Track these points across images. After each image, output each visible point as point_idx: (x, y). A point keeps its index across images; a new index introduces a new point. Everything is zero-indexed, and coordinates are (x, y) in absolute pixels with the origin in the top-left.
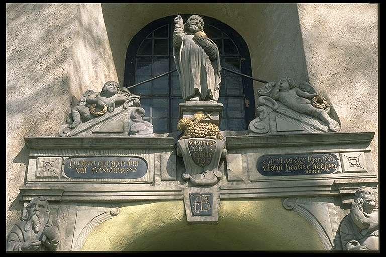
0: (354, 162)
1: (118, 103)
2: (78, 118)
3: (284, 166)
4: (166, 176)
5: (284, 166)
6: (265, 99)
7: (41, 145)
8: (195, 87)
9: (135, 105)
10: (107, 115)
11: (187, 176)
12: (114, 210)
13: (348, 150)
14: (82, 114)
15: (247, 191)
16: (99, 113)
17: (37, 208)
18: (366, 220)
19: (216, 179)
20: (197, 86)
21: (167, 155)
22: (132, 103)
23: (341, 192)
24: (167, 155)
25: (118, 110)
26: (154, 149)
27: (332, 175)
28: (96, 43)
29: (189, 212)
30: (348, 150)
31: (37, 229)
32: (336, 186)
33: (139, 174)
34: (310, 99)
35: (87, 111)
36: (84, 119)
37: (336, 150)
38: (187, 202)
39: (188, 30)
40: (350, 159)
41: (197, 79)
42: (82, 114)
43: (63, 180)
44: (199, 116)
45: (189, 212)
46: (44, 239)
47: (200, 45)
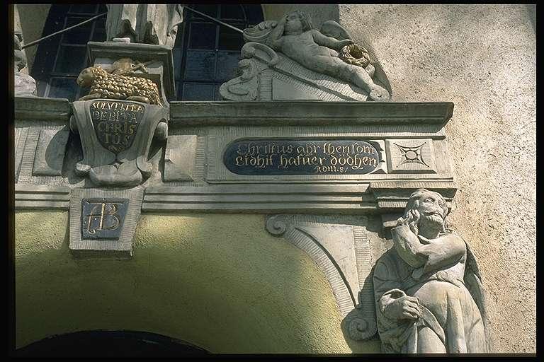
0: (412, 155)
3: (276, 159)
4: (43, 165)
5: (276, 159)
11: (82, 168)
18: (422, 249)
23: (382, 204)
34: (338, 48)
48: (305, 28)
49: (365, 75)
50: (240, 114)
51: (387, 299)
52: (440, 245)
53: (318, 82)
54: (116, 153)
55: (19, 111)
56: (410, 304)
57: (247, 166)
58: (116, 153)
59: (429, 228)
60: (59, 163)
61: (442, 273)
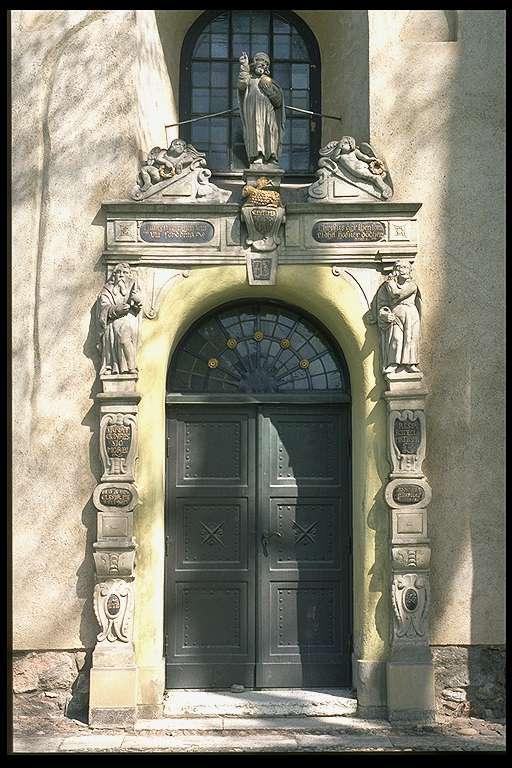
0: (400, 231)
1: (185, 165)
2: (148, 180)
3: (337, 234)
4: (231, 241)
5: (337, 234)
6: (326, 161)
7: (118, 210)
8: (259, 149)
9: (201, 166)
10: (176, 177)
11: (250, 242)
12: (186, 272)
13: (252, 610)
14: (152, 176)
15: (301, 258)
16: (168, 175)
17: (122, 274)
18: (398, 291)
19: (275, 246)
20: (261, 148)
21: (232, 220)
22: (198, 164)
23: (384, 260)
24: (232, 220)
25: (185, 171)
26: (216, 213)
27: (379, 243)
28: (90, 19)
29: (251, 277)
30: (252, 610)
31: (124, 292)
32: (379, 255)
33: (207, 238)
34: (368, 162)
35: (156, 172)
36: (154, 181)
37: (385, 219)
38: (250, 267)
39: (253, 72)
40: (398, 228)
41: (261, 140)
42: (152, 176)
43: (139, 244)
44: (263, 182)
45: (251, 277)
46: (132, 303)
47: (265, 94)
48: (352, 150)
49: (380, 179)
50: (320, 209)
51: (382, 312)
52: (406, 288)
53: (357, 184)
54: (264, 234)
55: (413, 356)
56: (391, 317)
57: (429, 405)
58: (264, 234)
59: (401, 280)
60: (238, 240)
61: (405, 301)
